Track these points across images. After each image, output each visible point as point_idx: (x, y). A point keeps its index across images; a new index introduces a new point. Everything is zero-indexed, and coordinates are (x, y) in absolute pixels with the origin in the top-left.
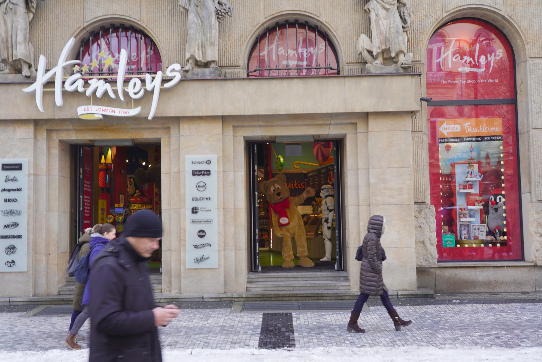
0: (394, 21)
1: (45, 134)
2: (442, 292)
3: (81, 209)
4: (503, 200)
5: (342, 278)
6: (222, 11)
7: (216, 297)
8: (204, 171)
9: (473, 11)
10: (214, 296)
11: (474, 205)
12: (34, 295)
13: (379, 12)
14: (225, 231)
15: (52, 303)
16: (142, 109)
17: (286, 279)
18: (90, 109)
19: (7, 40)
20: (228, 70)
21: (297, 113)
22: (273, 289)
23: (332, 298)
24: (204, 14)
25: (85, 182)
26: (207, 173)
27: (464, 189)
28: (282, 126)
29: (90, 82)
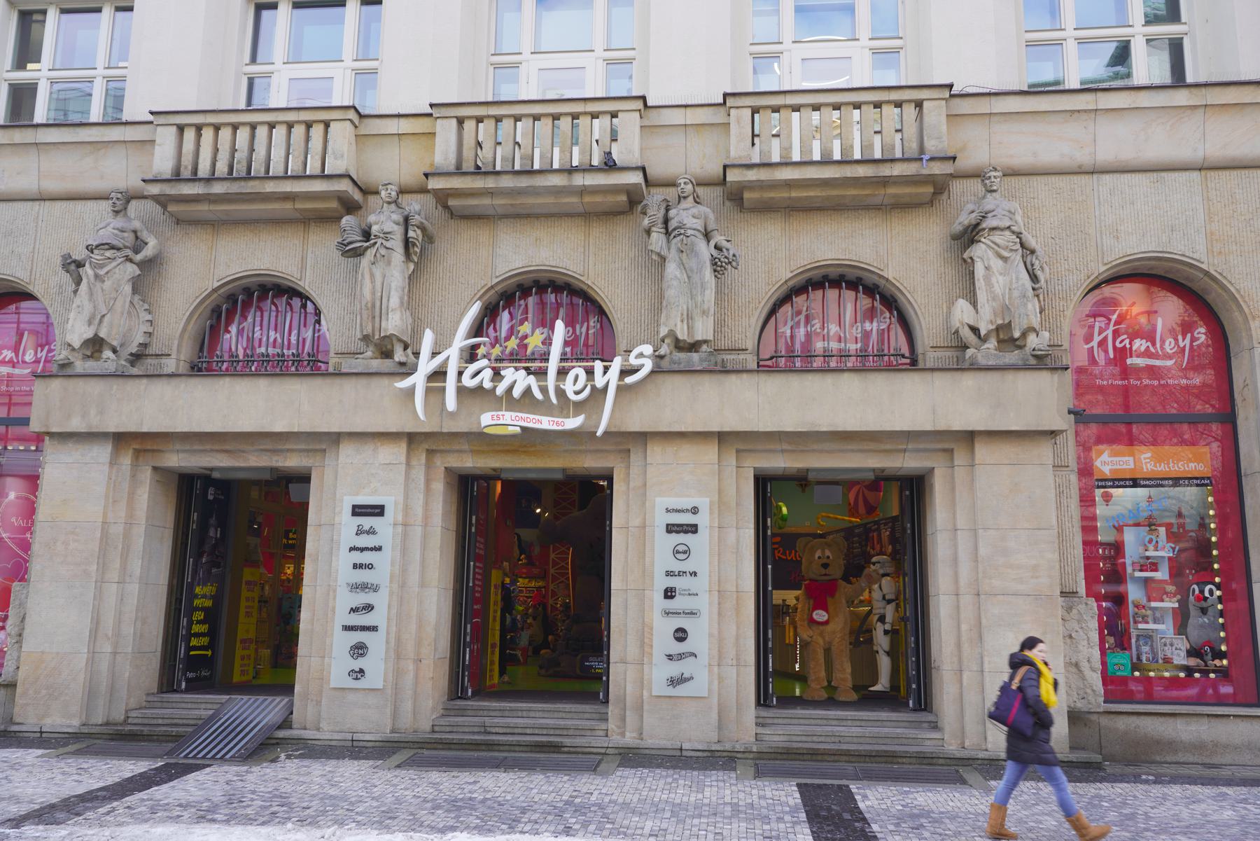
0: (1017, 278)
1: (423, 457)
2: (1112, 759)
3: (471, 584)
4: (1218, 593)
5: (925, 725)
6: (722, 259)
7: (705, 748)
8: (687, 525)
9: (1153, 263)
10: (700, 748)
11: (1162, 601)
12: (392, 731)
13: (992, 263)
14: (720, 632)
15: (423, 745)
16: (586, 419)
17: (825, 722)
18: (501, 417)
19: (373, 306)
20: (728, 357)
21: (849, 428)
22: (804, 739)
23: (913, 760)
24: (692, 263)
25: (479, 538)
26: (693, 529)
27: (1141, 570)
28: (821, 451)
29: (502, 373)
